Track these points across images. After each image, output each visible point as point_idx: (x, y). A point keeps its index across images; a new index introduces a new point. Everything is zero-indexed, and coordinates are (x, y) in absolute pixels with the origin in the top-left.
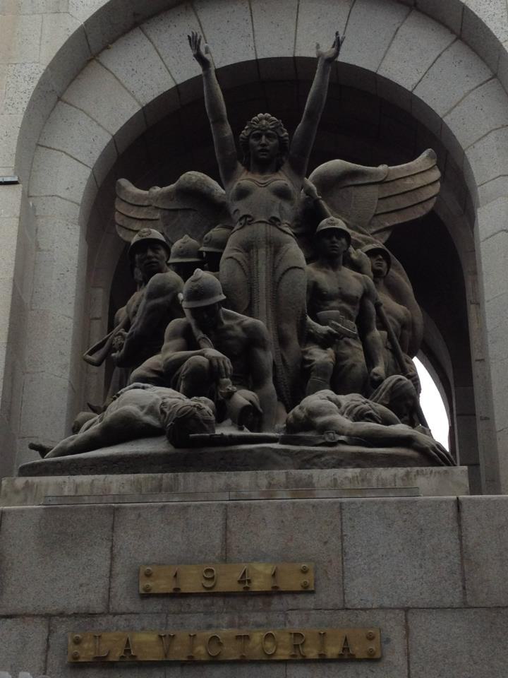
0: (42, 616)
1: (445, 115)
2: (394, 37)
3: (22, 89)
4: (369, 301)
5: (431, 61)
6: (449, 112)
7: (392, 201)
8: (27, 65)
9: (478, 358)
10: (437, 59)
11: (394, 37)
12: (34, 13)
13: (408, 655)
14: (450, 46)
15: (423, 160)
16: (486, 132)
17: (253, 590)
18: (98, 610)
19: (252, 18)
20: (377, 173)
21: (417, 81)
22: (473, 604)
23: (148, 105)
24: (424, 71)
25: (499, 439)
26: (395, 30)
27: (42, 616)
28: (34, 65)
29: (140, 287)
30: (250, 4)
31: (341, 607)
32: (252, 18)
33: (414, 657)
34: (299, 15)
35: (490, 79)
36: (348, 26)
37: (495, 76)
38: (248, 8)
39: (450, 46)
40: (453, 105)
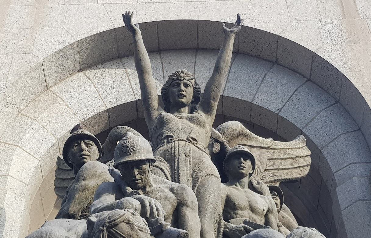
1: (303, 128)
2: (263, 80)
4: (272, 217)
5: (290, 94)
6: (307, 125)
7: (276, 162)
10: (295, 92)
11: (263, 80)
12: (7, 54)
14: (304, 84)
16: (336, 136)
17: (311, 162)
19: (163, 69)
21: (281, 106)
26: (264, 75)
29: (118, 174)
30: (162, 61)
32: (163, 69)
34: (196, 67)
35: (335, 104)
36: (230, 73)
37: (338, 102)
38: (160, 63)
39: (304, 84)
40: (309, 120)
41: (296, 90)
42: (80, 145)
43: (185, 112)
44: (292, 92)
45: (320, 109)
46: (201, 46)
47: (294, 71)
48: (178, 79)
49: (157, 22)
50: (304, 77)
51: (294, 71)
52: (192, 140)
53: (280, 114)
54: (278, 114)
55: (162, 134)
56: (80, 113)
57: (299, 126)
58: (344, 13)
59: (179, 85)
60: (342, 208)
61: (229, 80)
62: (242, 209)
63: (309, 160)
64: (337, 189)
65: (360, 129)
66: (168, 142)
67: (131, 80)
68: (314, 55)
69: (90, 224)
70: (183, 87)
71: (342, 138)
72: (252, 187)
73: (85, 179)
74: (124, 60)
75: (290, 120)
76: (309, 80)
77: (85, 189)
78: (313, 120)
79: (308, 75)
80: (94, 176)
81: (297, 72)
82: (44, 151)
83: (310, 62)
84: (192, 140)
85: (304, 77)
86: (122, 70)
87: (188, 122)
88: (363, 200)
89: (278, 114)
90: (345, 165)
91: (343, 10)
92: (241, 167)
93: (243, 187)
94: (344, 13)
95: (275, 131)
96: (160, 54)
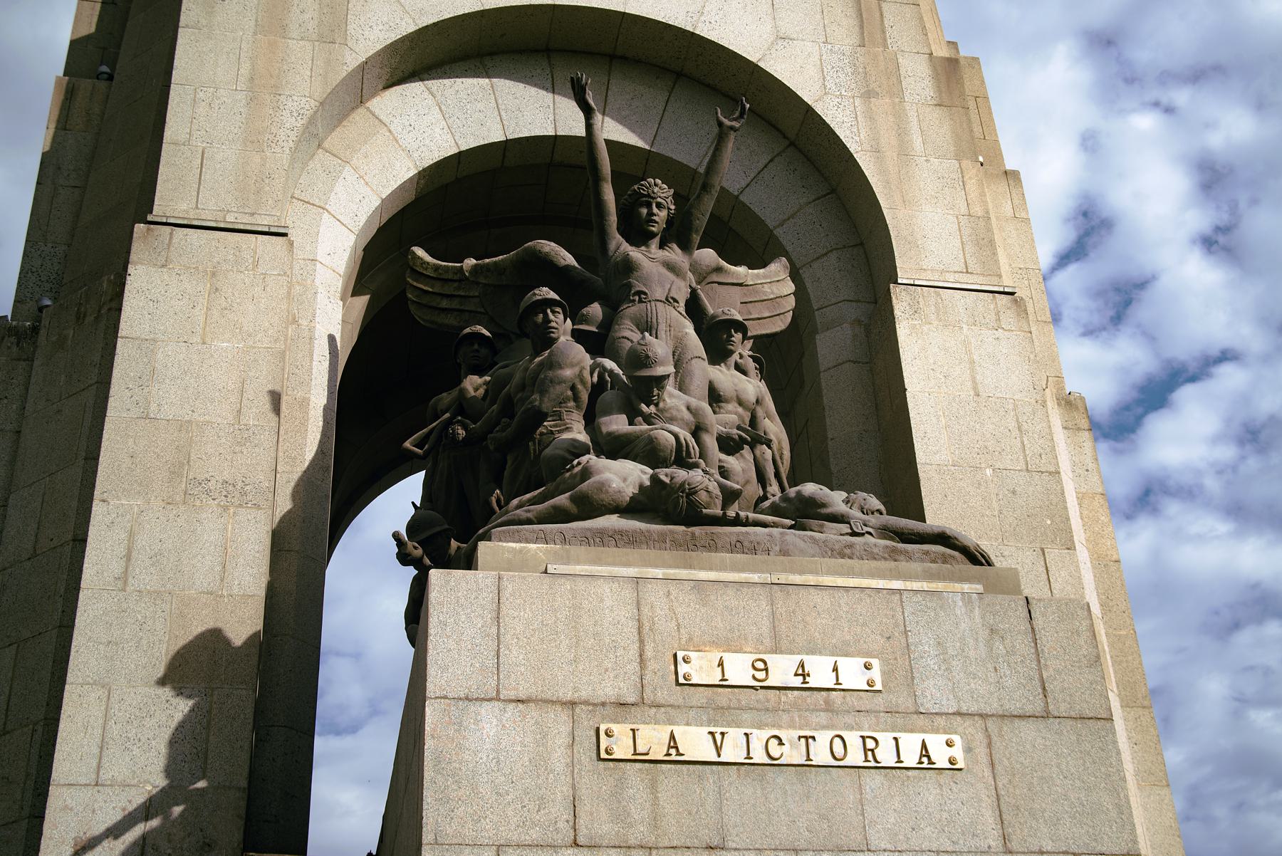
0: (564, 704)
3: (288, 125)
5: (761, 165)
8: (295, 98)
9: (505, 583)
12: (302, 39)
13: (992, 765)
14: (784, 151)
15: (778, 269)
18: (631, 700)
20: (738, 275)
21: (744, 184)
22: (1056, 714)
23: (424, 170)
24: (752, 175)
25: (124, 810)
27: (564, 704)
28: (304, 100)
31: (912, 709)
33: (999, 768)
37: (833, 191)
39: (784, 151)
41: (771, 161)
42: (546, 315)
43: (655, 243)
44: (765, 162)
48: (649, 196)
49: (554, 6)
53: (741, 198)
54: (737, 197)
55: (629, 286)
56: (416, 155)
57: (768, 222)
59: (649, 205)
60: (822, 368)
64: (817, 337)
65: (862, 244)
66: (640, 301)
67: (500, 101)
68: (809, 110)
69: (654, 479)
70: (655, 210)
71: (833, 256)
72: (738, 368)
73: (561, 368)
75: (756, 210)
76: (792, 144)
78: (792, 216)
81: (774, 126)
85: (785, 137)
87: (664, 271)
88: (855, 362)
89: (737, 197)
90: (834, 300)
91: (862, 27)
92: (729, 341)
93: (729, 369)
96: (549, 57)
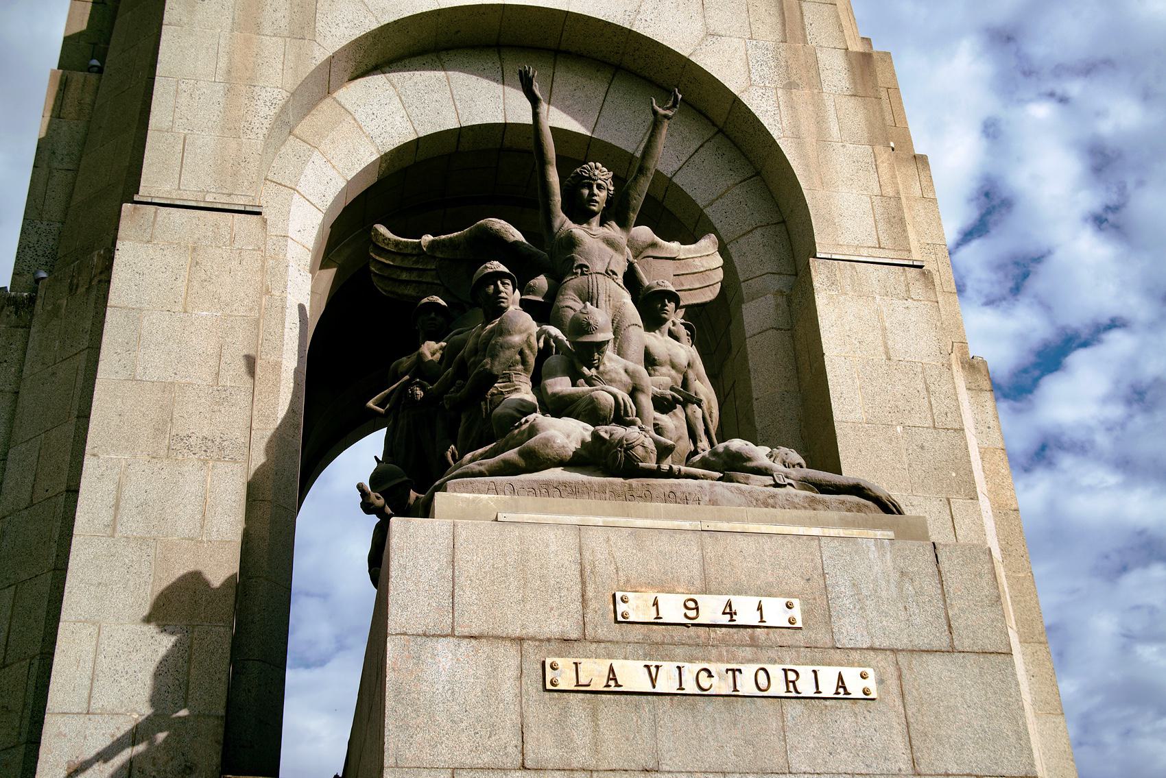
5: (692, 150)
6: (711, 204)
12: (275, 35)
14: (712, 137)
21: (676, 168)
37: (758, 174)
39: (712, 137)
41: (702, 146)
43: (595, 221)
45: (730, 183)
46: (562, 47)
47: (700, 112)
48: (590, 178)
50: (714, 124)
51: (700, 112)
52: (610, 273)
53: (674, 180)
54: (670, 179)
55: (573, 260)
56: (378, 141)
57: (699, 202)
58: (784, 30)
59: (590, 187)
61: (603, 113)
62: (661, 365)
63: (720, 275)
65: (784, 222)
66: (582, 274)
68: (736, 100)
69: (595, 435)
71: (758, 233)
74: (443, 56)
75: (688, 191)
76: (720, 131)
77: (510, 347)
78: (720, 197)
79: (720, 124)
80: (521, 332)
82: (330, 199)
83: (728, 107)
84: (610, 273)
85: (714, 124)
86: (440, 74)
89: (670, 179)
90: (758, 273)
91: (784, 25)
92: (663, 309)
94: (784, 30)
95: (660, 198)
96: (499, 53)
